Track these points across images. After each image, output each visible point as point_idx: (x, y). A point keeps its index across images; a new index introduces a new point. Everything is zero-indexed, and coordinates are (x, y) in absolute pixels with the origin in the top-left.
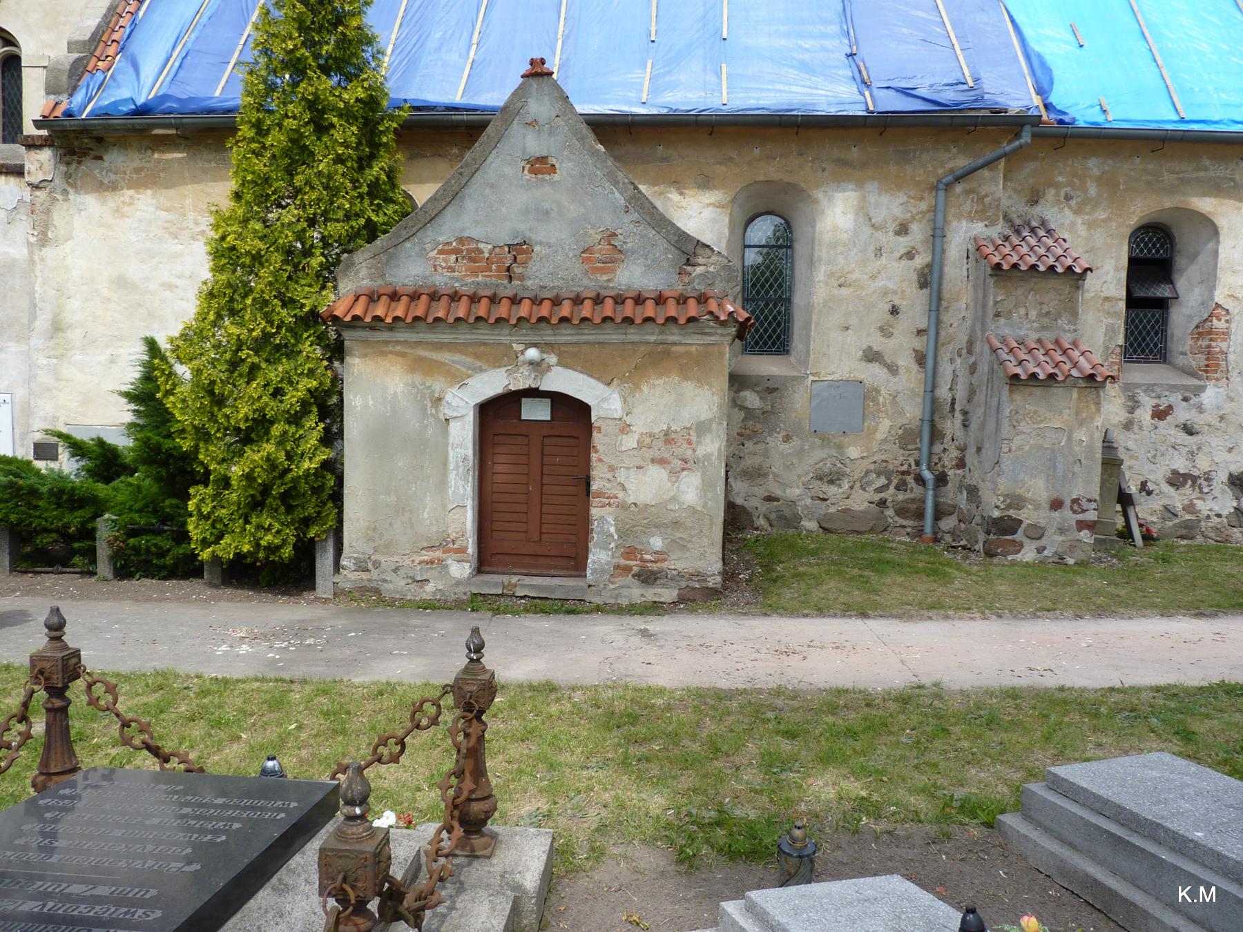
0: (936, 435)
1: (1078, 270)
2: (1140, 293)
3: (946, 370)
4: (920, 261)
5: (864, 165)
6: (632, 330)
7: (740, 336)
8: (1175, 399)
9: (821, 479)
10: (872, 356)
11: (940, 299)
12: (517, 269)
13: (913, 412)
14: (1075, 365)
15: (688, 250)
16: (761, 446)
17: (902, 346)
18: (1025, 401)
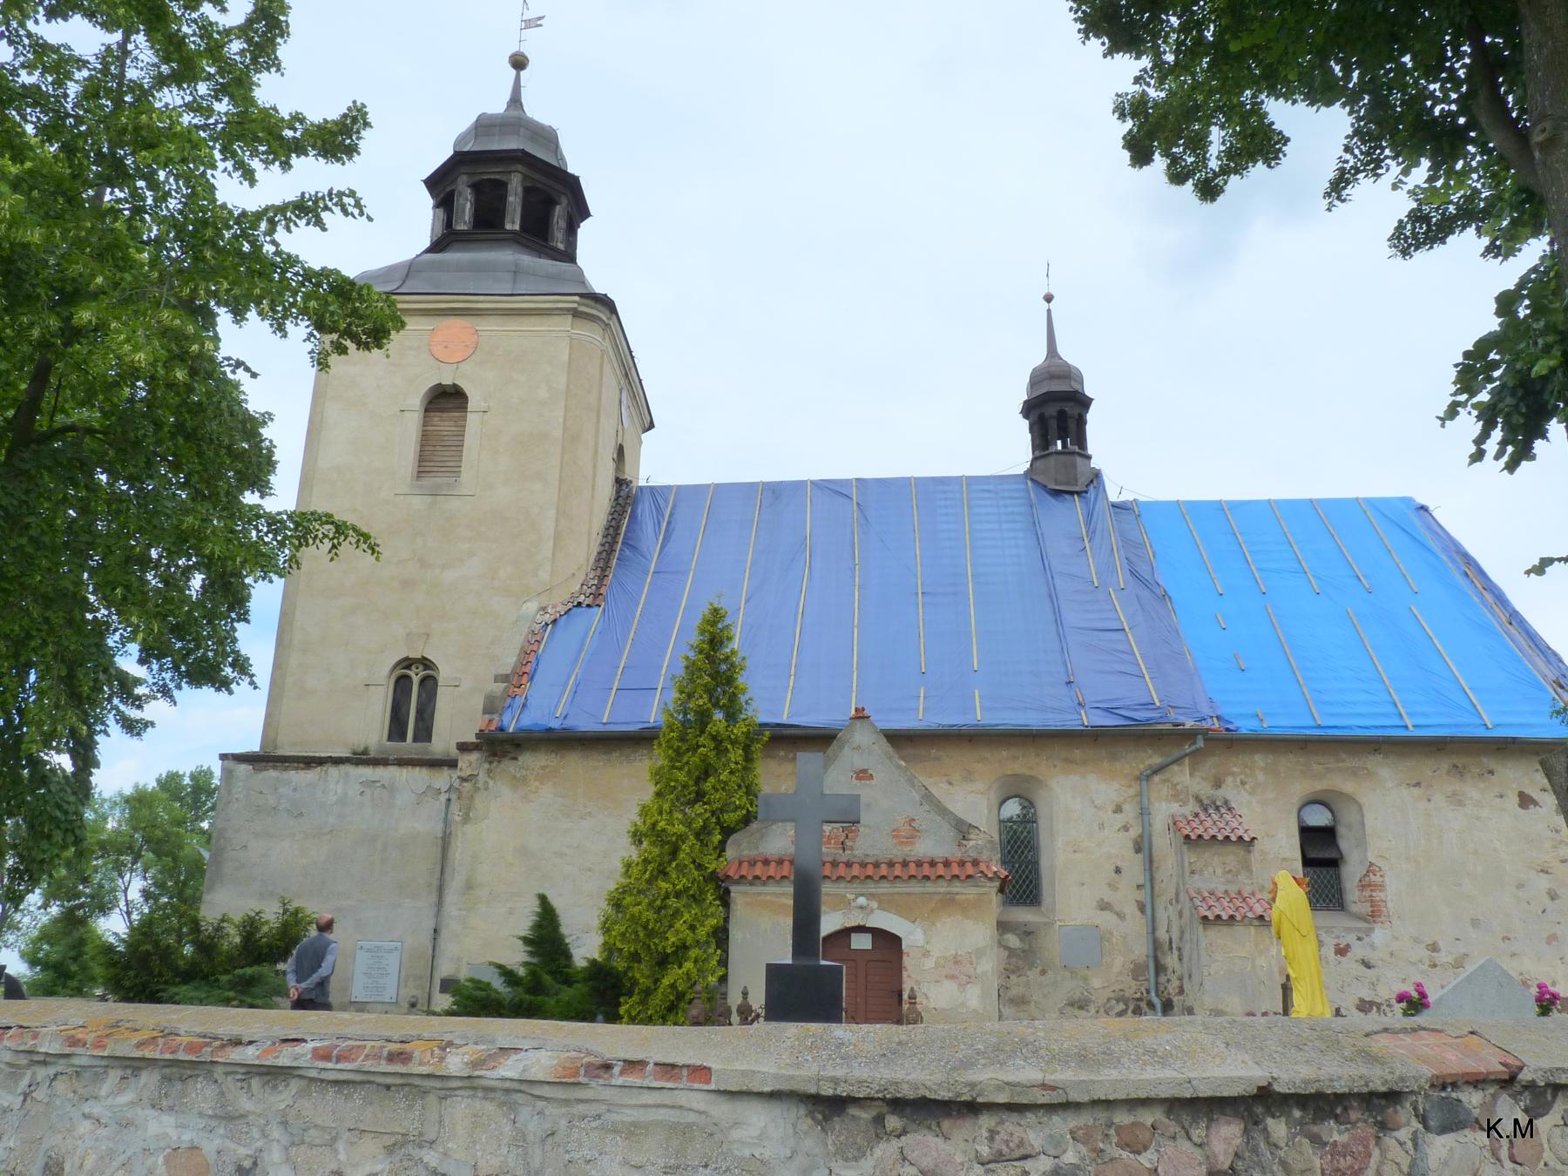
0: (1160, 968)
1: (1247, 839)
2: (1313, 855)
3: (1162, 917)
4: (1134, 832)
5: (1084, 763)
6: (928, 884)
7: (1001, 890)
8: (1350, 939)
9: (1072, 1005)
10: (1104, 906)
11: (1151, 861)
12: (849, 843)
13: (1141, 951)
14: (1251, 909)
15: (963, 830)
16: (1023, 979)
17: (1126, 897)
18: (1215, 935)
